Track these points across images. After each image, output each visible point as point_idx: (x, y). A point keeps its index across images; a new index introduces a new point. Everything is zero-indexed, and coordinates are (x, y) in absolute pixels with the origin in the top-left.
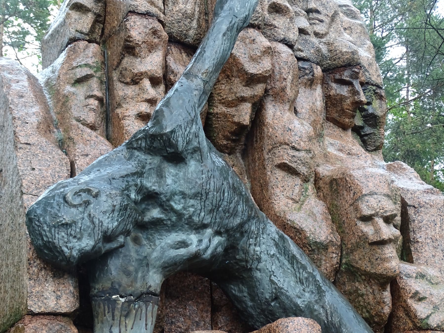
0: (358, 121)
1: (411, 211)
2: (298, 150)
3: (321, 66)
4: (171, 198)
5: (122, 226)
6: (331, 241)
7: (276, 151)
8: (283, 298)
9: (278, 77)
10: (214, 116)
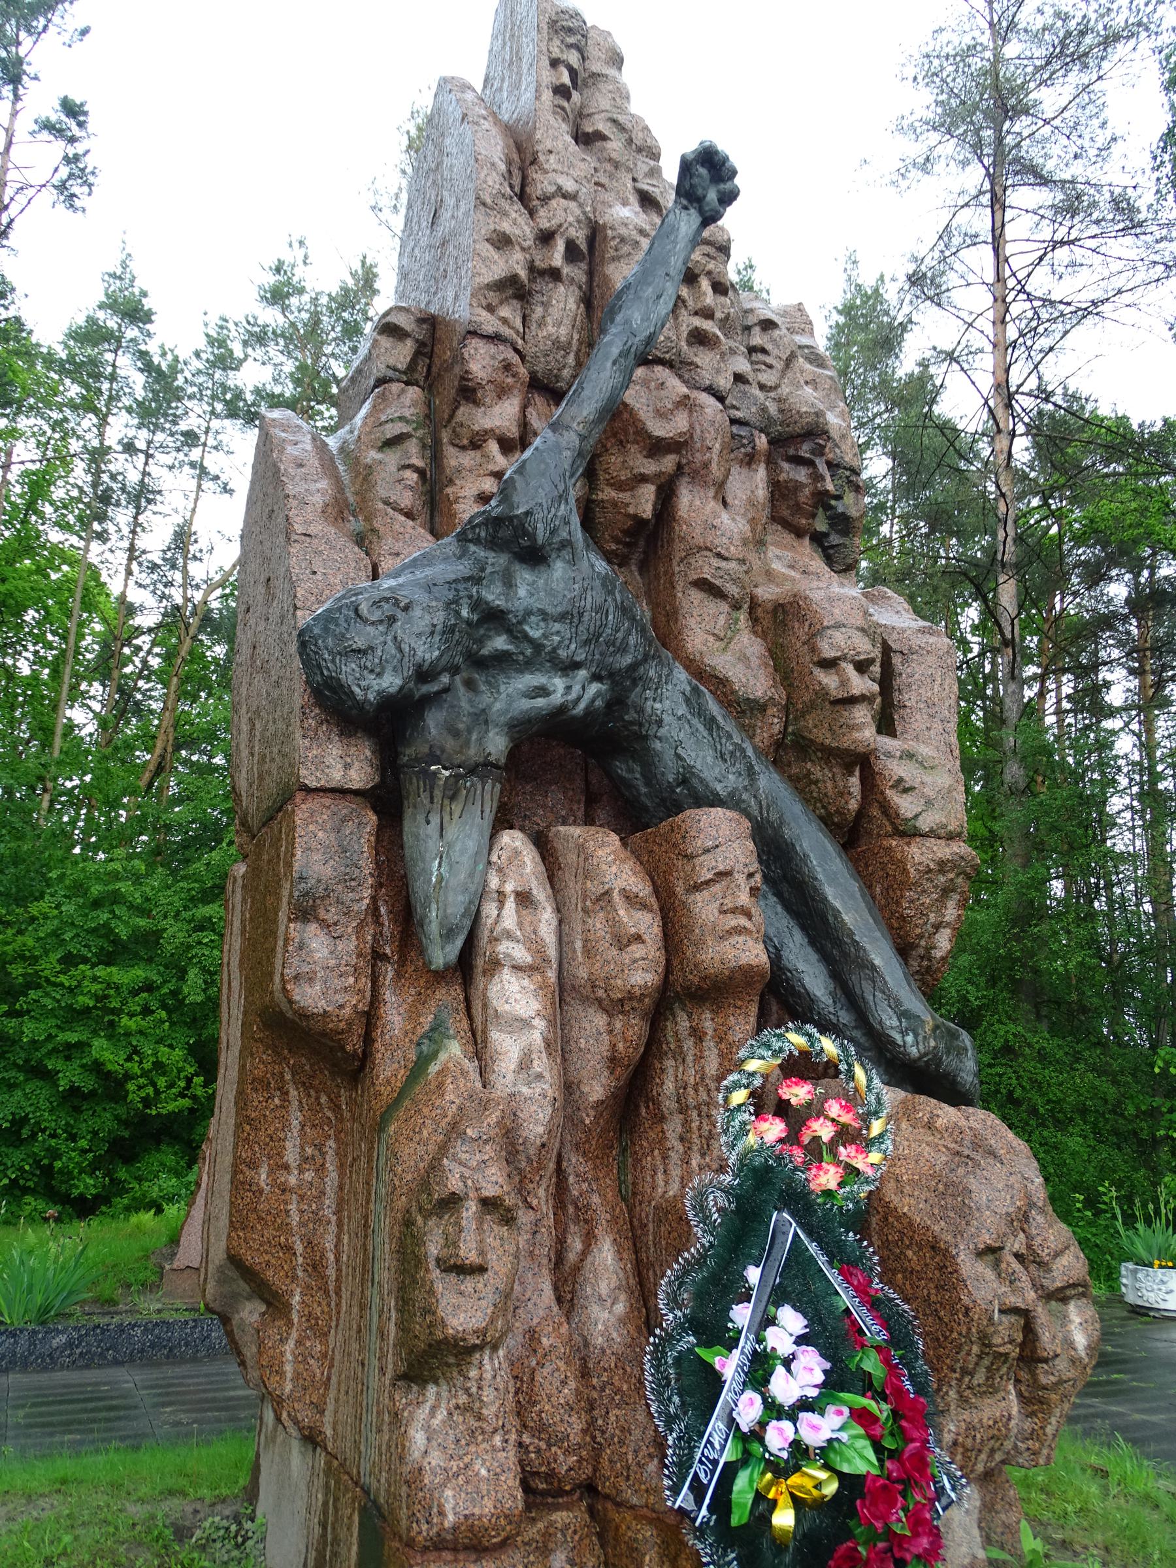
0: (821, 525)
1: (897, 660)
2: (726, 559)
3: (767, 434)
5: (446, 658)
7: (692, 561)
8: (694, 781)
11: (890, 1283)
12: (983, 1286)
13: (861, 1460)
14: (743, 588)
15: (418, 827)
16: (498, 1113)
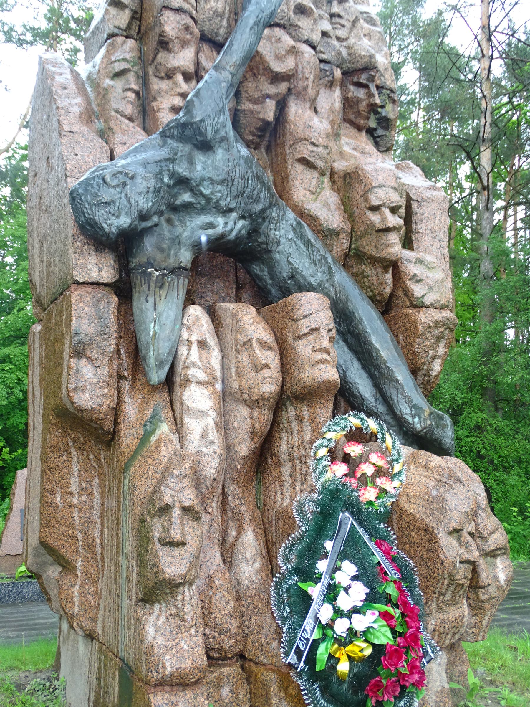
0: (372, 124)
1: (414, 205)
2: (316, 146)
3: (341, 69)
4: (200, 183)
5: (156, 207)
6: (342, 228)
7: (297, 147)
8: (298, 277)
9: (300, 76)
10: (242, 113)
11: (403, 549)
12: (451, 549)
13: (384, 636)
14: (327, 163)
15: (141, 304)
16: (190, 462)
